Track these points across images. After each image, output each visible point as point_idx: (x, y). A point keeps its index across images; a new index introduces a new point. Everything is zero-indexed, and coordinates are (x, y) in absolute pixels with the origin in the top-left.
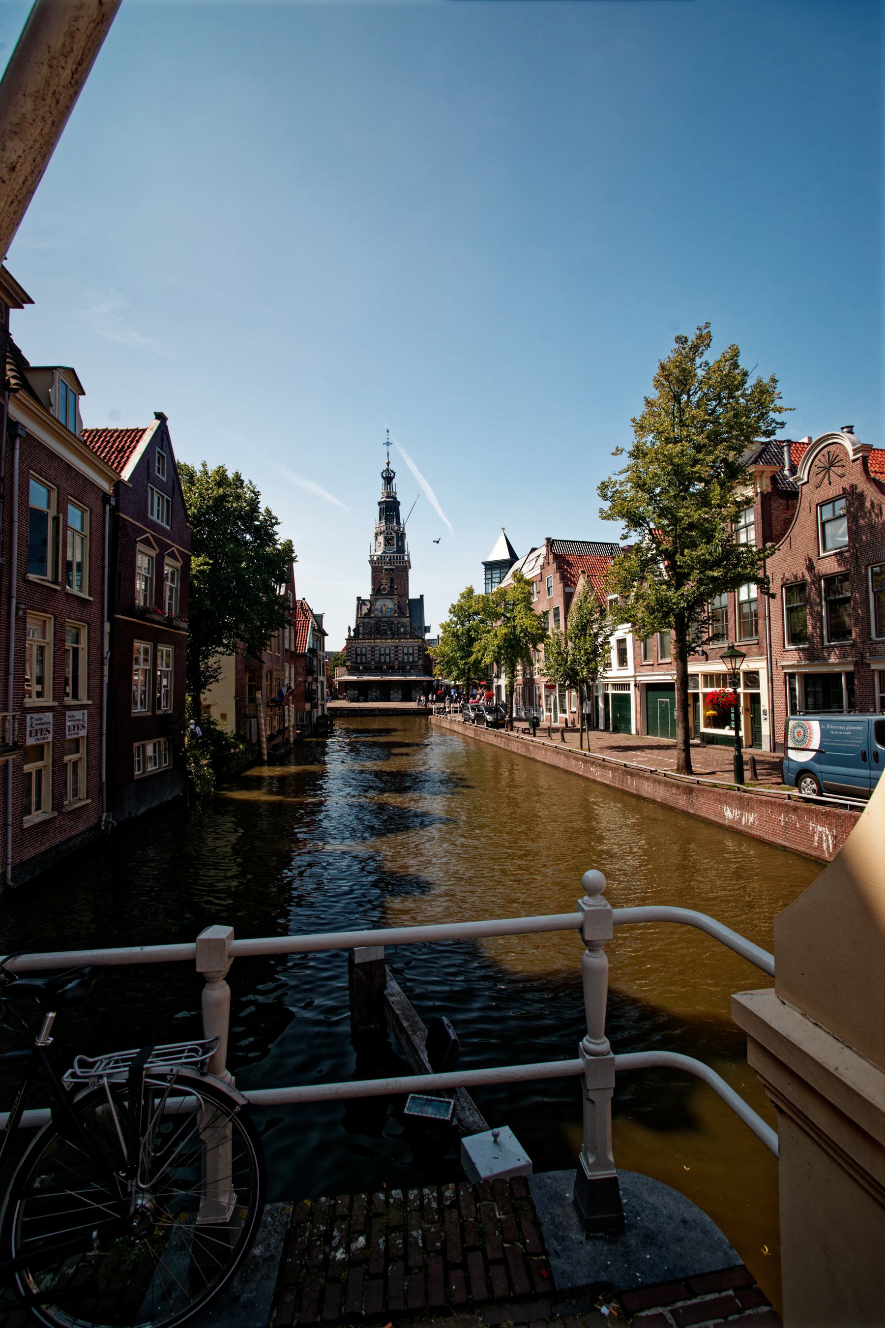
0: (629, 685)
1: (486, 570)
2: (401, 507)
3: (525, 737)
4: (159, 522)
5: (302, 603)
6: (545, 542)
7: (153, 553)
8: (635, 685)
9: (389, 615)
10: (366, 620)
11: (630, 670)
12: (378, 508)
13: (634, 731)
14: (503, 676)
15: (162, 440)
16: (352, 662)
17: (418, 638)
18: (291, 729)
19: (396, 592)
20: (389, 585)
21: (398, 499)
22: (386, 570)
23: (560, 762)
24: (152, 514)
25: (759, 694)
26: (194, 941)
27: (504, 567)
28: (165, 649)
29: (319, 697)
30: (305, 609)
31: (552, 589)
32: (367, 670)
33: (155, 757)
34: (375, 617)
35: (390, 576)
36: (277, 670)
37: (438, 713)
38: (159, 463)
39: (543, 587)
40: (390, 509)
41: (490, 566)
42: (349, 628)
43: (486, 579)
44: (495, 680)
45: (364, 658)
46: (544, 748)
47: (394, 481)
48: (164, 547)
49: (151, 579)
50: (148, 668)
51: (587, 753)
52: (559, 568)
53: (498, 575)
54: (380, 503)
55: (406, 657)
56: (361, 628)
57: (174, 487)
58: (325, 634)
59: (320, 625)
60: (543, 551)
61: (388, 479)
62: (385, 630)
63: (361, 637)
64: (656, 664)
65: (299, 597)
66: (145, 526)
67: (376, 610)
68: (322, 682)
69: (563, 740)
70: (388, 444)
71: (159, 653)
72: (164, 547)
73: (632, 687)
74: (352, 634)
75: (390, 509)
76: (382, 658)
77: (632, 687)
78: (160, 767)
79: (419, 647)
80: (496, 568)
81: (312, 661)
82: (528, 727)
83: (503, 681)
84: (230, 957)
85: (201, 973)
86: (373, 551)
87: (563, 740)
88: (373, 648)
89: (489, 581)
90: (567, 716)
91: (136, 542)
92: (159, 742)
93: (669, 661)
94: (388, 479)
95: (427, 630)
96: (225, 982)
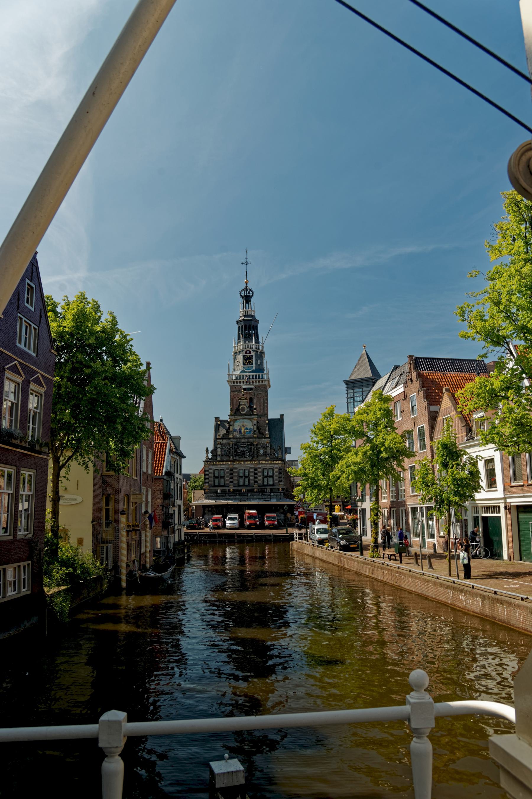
0: (499, 507)
1: (348, 388)
2: (259, 326)
3: (392, 563)
4: (26, 349)
5: (159, 425)
6: (408, 360)
7: (20, 380)
8: (506, 508)
9: (248, 435)
10: (225, 441)
11: (499, 493)
12: (236, 327)
13: (505, 557)
14: (367, 498)
15: (32, 273)
16: (210, 486)
17: (278, 459)
18: (148, 555)
19: (255, 412)
20: (248, 405)
21: (257, 318)
22: (245, 389)
23: (430, 591)
24: (20, 343)
25: (500, 517)
26: (97, 723)
27: (367, 386)
28: (27, 473)
29: (176, 522)
30: (164, 433)
31: (416, 408)
32: (225, 494)
33: (15, 582)
34: (233, 438)
35: (248, 396)
36: (134, 494)
37: (301, 538)
38: (28, 294)
39: (407, 406)
40: (248, 328)
41: (351, 384)
42: (207, 450)
43: (348, 398)
44: (359, 503)
45: (222, 480)
46: (411, 575)
47: (253, 300)
48: (29, 373)
49: (17, 404)
50: (11, 492)
51: (456, 580)
52: (423, 386)
53: (361, 394)
54: (238, 322)
55: (266, 480)
56: (219, 450)
57: (41, 317)
58: (182, 456)
59: (177, 447)
60: (407, 368)
61: (247, 299)
62: (244, 451)
63: (219, 458)
64: (526, 484)
65: (156, 419)
66: (13, 354)
67: (235, 430)
68: (179, 506)
69: (431, 566)
70: (246, 263)
71: (22, 477)
72: (29, 373)
73: (502, 509)
74: (210, 456)
75: (248, 328)
76: (241, 480)
77: (502, 509)
78: (19, 592)
79: (280, 469)
80: (358, 387)
81: (168, 485)
82: (394, 553)
83: (367, 505)
84: (124, 736)
85: (101, 748)
86: (231, 370)
87: (431, 566)
88: (231, 470)
89: (351, 400)
90: (435, 541)
91: (4, 370)
92: (19, 566)
93: (521, 484)
94: (247, 299)
95: (288, 450)
96: (120, 758)
